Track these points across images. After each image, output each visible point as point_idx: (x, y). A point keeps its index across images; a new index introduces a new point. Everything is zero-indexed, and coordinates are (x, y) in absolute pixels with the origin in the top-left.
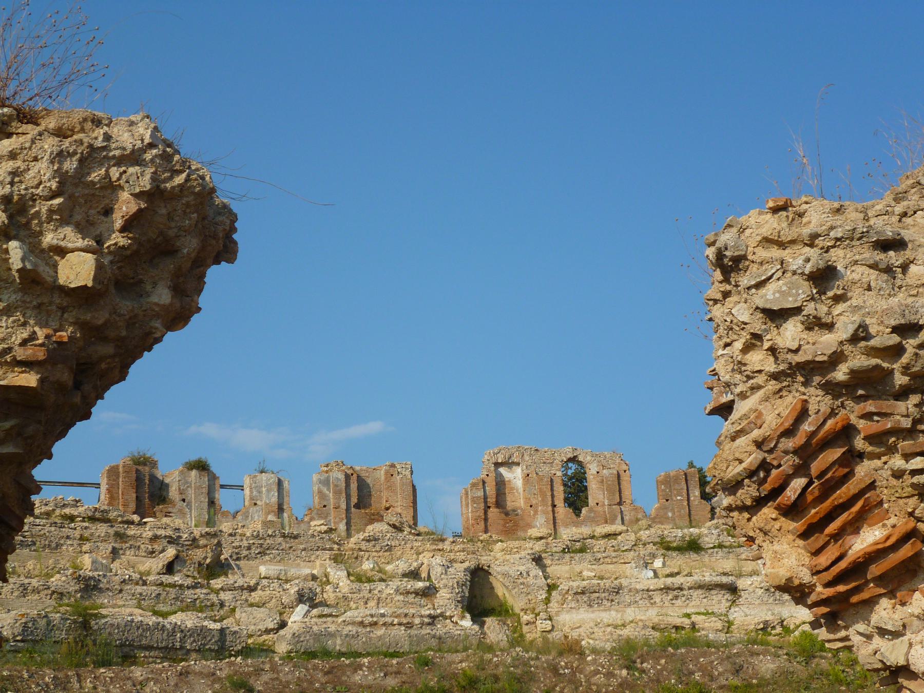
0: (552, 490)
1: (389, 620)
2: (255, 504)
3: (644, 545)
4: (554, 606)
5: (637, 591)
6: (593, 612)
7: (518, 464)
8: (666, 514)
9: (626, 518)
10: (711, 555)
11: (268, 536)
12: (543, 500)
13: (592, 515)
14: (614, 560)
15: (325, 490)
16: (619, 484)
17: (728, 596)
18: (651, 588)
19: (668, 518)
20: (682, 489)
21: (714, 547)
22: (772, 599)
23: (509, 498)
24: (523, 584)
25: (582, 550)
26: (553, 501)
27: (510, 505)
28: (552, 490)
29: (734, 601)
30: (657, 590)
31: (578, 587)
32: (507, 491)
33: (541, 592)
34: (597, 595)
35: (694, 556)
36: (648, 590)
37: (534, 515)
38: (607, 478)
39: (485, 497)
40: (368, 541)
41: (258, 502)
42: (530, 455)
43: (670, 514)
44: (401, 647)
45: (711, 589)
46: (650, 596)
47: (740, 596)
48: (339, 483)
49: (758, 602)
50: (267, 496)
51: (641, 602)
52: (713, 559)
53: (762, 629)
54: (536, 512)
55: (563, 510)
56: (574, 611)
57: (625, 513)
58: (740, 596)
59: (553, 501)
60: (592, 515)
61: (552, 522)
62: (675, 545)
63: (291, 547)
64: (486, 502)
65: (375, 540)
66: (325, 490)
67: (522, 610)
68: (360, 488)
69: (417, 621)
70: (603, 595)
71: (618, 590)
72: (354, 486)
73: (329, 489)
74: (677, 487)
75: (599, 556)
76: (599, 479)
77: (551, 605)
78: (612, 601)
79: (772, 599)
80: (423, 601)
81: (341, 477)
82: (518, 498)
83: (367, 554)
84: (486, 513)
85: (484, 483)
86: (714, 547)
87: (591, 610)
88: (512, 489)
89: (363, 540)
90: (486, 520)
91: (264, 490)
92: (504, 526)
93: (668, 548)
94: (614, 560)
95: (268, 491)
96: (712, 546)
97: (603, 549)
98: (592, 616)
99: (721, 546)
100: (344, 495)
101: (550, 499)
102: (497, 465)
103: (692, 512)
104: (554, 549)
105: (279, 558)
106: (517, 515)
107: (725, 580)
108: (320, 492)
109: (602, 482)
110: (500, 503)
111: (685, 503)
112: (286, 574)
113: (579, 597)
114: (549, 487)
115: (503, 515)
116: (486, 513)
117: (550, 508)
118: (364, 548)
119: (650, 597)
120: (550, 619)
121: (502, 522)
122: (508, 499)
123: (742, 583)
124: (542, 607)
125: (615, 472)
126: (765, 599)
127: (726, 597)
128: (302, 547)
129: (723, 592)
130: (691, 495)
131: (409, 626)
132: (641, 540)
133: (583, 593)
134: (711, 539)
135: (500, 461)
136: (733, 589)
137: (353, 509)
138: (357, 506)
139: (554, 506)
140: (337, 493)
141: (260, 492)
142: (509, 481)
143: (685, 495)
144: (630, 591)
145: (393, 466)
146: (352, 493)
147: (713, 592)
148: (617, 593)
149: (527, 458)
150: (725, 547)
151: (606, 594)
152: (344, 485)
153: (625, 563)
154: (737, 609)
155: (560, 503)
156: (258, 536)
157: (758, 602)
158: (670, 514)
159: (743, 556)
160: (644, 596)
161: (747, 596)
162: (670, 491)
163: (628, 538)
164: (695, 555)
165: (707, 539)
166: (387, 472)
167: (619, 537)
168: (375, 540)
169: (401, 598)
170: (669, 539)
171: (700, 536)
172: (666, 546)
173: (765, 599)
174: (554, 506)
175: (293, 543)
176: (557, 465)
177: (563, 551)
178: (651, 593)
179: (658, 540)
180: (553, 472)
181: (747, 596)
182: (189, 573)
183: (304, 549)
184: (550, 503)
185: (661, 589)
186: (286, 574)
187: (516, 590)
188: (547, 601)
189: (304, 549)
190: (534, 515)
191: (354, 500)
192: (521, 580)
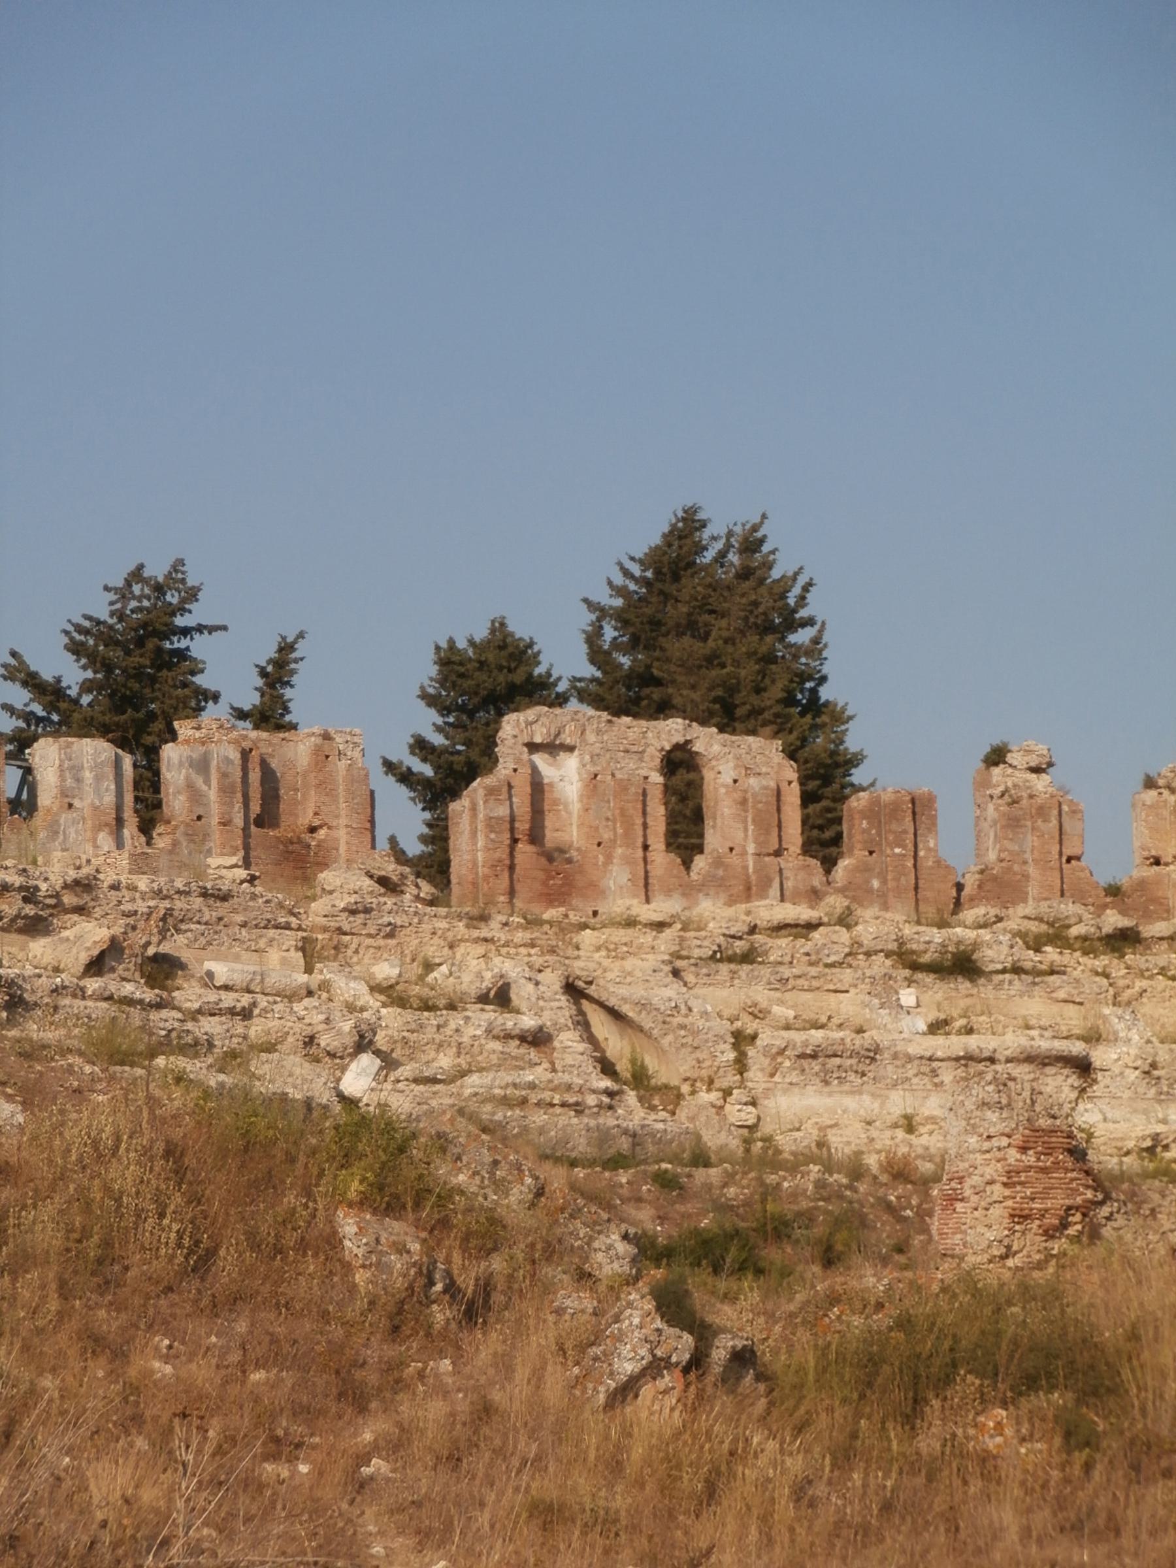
0: (644, 813)
1: (546, 1095)
2: (70, 806)
3: (868, 954)
4: (756, 1076)
5: (910, 1059)
6: (830, 1094)
7: (571, 749)
8: (868, 882)
9: (789, 884)
10: (999, 986)
11: (179, 892)
12: (627, 834)
13: (720, 872)
14: (815, 983)
15: (199, 782)
16: (779, 810)
17: (1074, 1080)
18: (939, 1054)
19: (870, 891)
20: (905, 832)
21: (1004, 971)
22: (1153, 1091)
23: (549, 822)
24: (682, 1027)
25: (748, 958)
26: (645, 836)
27: (551, 837)
28: (644, 813)
29: (1083, 1090)
30: (949, 1059)
31: (806, 1044)
32: (546, 808)
33: (722, 1047)
34: (837, 1061)
35: (964, 985)
36: (930, 1059)
37: (606, 864)
38: (754, 795)
39: (512, 820)
40: (353, 912)
41: (77, 803)
42: (599, 732)
43: (876, 884)
44: (573, 1150)
45: (1045, 1065)
46: (933, 1071)
47: (1095, 1081)
48: (230, 770)
49: (1127, 1094)
50: (97, 791)
51: (915, 1080)
52: (1002, 995)
53: (1148, 1149)
54: (609, 858)
55: (662, 859)
56: (796, 1090)
57: (786, 873)
58: (1095, 1081)
59: (645, 836)
60: (720, 872)
61: (642, 883)
62: (926, 959)
63: (220, 919)
64: (512, 830)
65: (367, 911)
66: (199, 782)
67: (686, 1080)
68: (263, 782)
69: (591, 1100)
70: (849, 1062)
71: (872, 1054)
72: (255, 776)
73: (207, 782)
74: (894, 826)
75: (786, 972)
76: (737, 796)
77: (749, 1075)
78: (863, 1074)
79: (1153, 1091)
80: (533, 1054)
81: (235, 755)
82: (569, 825)
83: (356, 940)
84: (512, 855)
85: (510, 787)
86: (1004, 971)
87: (826, 1089)
88: (556, 802)
89: (344, 910)
90: (512, 868)
91: (88, 775)
92: (545, 883)
93: (915, 967)
94: (815, 983)
95: (98, 779)
96: (1000, 967)
97: (787, 959)
98: (829, 1101)
99: (1017, 970)
100: (239, 795)
101: (640, 833)
102: (533, 747)
103: (921, 883)
104: (697, 953)
105: (203, 941)
106: (569, 861)
107: (1061, 1046)
108: (190, 786)
109: (744, 802)
110: (536, 836)
111: (910, 864)
112: (262, 981)
113: (805, 1063)
114: (640, 806)
115: (543, 860)
116: (512, 855)
117: (640, 853)
118: (346, 928)
119: (934, 1073)
120: (754, 1103)
121: (541, 875)
122: (547, 823)
123: (1100, 1056)
124: (732, 1079)
125: (773, 784)
126: (1141, 1090)
127: (1070, 1081)
128: (239, 918)
129: (1066, 1071)
130: (920, 846)
131: (578, 1108)
132: (860, 945)
133: (814, 1056)
134: (999, 952)
135: (538, 739)
136: (1083, 1067)
137: (252, 827)
138: (260, 822)
139: (646, 847)
140: (226, 790)
141: (78, 780)
142: (551, 785)
143: (911, 846)
144: (895, 1056)
145: (326, 737)
146: (251, 794)
147: (1050, 1070)
148: (873, 1059)
149: (591, 737)
150: (1026, 972)
151: (854, 1061)
152: (239, 773)
153: (836, 991)
154: (1089, 1106)
155: (658, 843)
156: (160, 891)
157: (1127, 1094)
158: (876, 884)
159: (1061, 994)
160: (923, 1069)
161: (1108, 1081)
162: (879, 834)
163: (835, 938)
164: (968, 984)
165: (989, 953)
166: (317, 750)
167: (816, 935)
168: (367, 911)
169: (497, 1046)
170: (914, 947)
171: (976, 945)
172: (910, 961)
173: (1141, 1090)
174: (646, 847)
175: (222, 909)
176: (652, 757)
177: (712, 957)
178: (935, 1064)
179: (893, 946)
180: (644, 773)
181: (1108, 1081)
182: (126, 974)
183: (244, 925)
184: (640, 840)
185: (957, 1059)
186: (262, 981)
187: (670, 1038)
188: (741, 1065)
189: (244, 925)
190: (606, 864)
191: (256, 808)
192: (678, 1020)
